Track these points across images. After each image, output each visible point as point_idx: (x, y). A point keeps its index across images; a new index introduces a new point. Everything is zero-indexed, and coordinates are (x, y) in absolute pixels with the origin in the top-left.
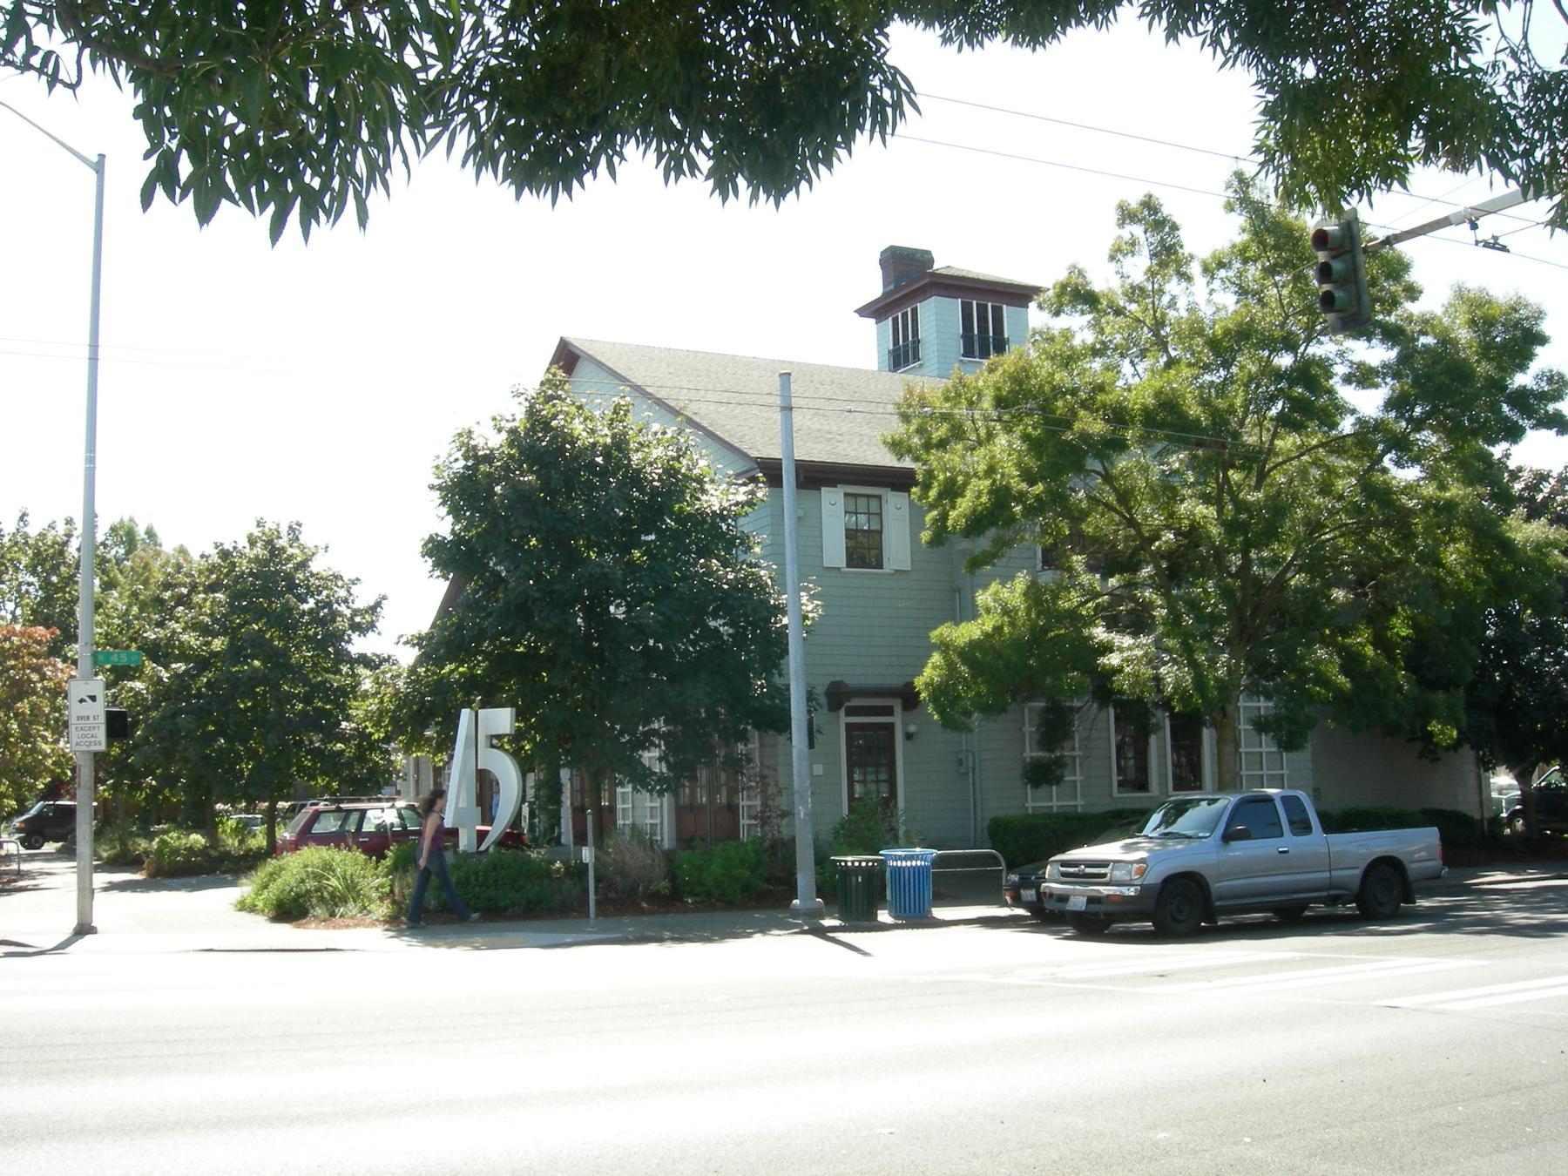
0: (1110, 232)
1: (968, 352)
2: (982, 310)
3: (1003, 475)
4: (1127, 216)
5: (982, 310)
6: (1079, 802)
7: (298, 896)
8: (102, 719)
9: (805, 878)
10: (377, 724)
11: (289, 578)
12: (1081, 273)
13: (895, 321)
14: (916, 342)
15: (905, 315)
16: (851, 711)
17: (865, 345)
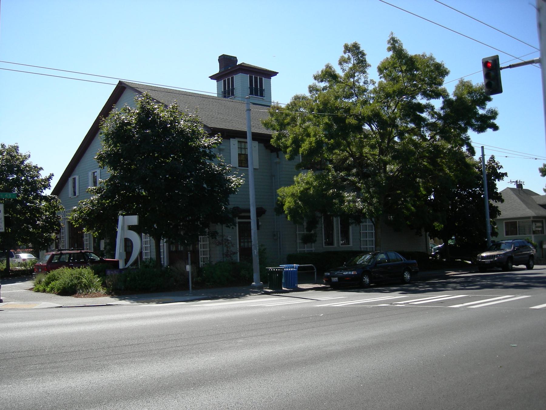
0: (340, 53)
1: (251, 93)
2: (256, 78)
3: (319, 136)
4: (347, 49)
5: (256, 78)
6: (313, 249)
7: (72, 285)
8: (3, 219)
9: (256, 276)
10: (76, 221)
11: (18, 167)
12: (330, 68)
13: (225, 81)
14: (233, 89)
15: (228, 80)
16: (240, 218)
17: (212, 89)
